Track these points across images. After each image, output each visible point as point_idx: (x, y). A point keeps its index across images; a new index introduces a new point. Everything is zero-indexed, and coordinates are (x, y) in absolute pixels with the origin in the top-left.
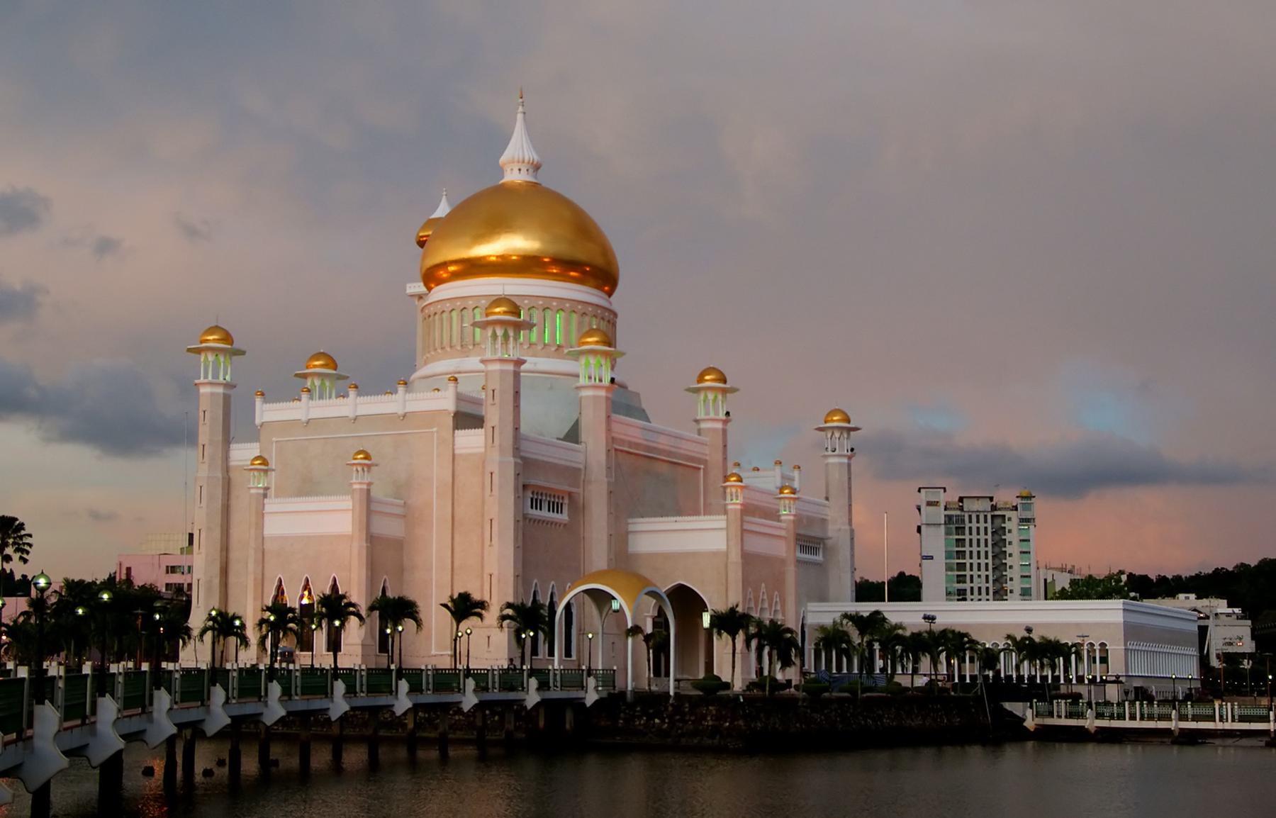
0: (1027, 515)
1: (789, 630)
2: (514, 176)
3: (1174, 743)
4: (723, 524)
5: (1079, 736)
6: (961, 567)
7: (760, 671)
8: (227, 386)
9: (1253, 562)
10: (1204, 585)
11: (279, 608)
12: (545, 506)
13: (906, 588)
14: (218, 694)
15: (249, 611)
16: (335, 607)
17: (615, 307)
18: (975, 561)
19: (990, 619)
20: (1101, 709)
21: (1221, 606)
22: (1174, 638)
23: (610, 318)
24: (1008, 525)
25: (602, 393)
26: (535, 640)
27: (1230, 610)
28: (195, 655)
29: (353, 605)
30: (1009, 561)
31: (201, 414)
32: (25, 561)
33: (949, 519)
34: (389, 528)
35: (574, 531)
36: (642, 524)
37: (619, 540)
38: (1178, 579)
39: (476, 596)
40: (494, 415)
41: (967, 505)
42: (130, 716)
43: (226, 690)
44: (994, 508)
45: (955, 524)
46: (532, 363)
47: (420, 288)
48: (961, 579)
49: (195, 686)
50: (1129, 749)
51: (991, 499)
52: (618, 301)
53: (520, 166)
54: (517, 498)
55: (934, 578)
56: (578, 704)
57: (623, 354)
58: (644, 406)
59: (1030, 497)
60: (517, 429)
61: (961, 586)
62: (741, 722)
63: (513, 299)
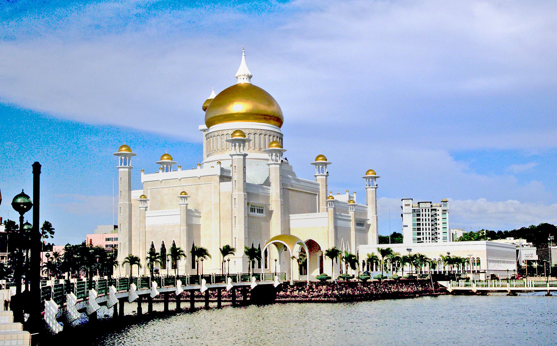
1: (354, 256)
5: (468, 293)
6: (419, 229)
7: (341, 272)
9: (537, 225)
10: (516, 234)
11: (152, 252)
12: (256, 211)
13: (397, 238)
14: (133, 286)
15: (142, 254)
17: (282, 132)
19: (434, 251)
20: (478, 283)
21: (524, 241)
22: (506, 255)
26: (428, 285)
27: (527, 244)
28: (119, 272)
29: (182, 251)
31: (120, 179)
32: (52, 237)
37: (286, 223)
38: (506, 232)
39: (231, 247)
40: (237, 176)
42: (101, 297)
43: (136, 285)
45: (417, 213)
47: (205, 127)
48: (419, 234)
49: (126, 283)
51: (431, 203)
52: (283, 130)
53: (244, 77)
54: (245, 208)
55: (408, 234)
57: (285, 151)
58: (294, 171)
61: (419, 237)
62: (336, 292)
63: (243, 131)
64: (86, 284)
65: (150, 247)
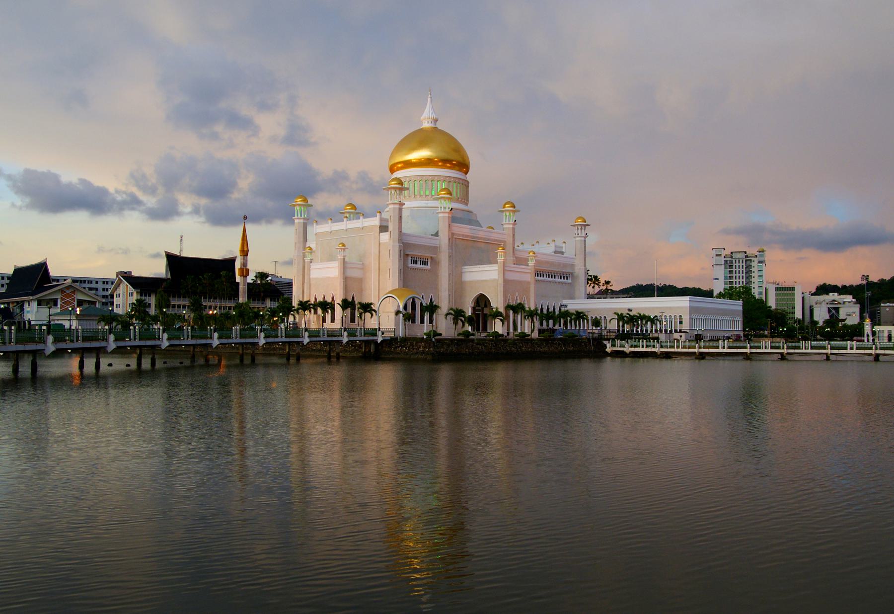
0: (761, 259)
2: (427, 125)
3: (696, 358)
4: (496, 268)
8: (304, 219)
16: (326, 306)
18: (737, 280)
23: (466, 184)
24: (753, 264)
25: (447, 215)
30: (753, 280)
33: (726, 262)
34: (351, 273)
35: (434, 272)
36: (467, 269)
41: (733, 255)
44: (746, 256)
46: (408, 204)
50: (727, 362)
56: (375, 342)
59: (763, 251)
60: (400, 232)
64: (483, 335)
65: (722, 300)
